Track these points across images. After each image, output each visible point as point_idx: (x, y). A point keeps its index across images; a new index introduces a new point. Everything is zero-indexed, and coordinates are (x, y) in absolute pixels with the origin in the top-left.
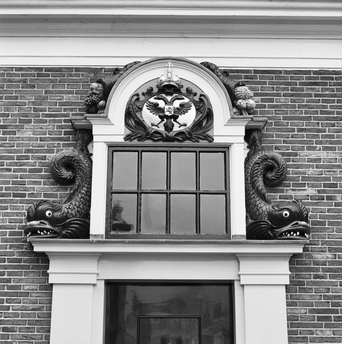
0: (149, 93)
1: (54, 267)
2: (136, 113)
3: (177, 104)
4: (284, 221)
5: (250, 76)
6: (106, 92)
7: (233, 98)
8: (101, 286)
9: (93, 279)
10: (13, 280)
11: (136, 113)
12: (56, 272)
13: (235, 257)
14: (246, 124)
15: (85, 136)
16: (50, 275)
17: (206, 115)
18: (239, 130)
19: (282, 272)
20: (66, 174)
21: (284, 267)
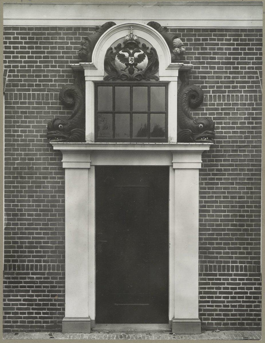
0: (119, 48)
3: (136, 55)
7: (172, 46)
9: (88, 166)
16: (67, 172)
17: (154, 63)
20: (69, 101)
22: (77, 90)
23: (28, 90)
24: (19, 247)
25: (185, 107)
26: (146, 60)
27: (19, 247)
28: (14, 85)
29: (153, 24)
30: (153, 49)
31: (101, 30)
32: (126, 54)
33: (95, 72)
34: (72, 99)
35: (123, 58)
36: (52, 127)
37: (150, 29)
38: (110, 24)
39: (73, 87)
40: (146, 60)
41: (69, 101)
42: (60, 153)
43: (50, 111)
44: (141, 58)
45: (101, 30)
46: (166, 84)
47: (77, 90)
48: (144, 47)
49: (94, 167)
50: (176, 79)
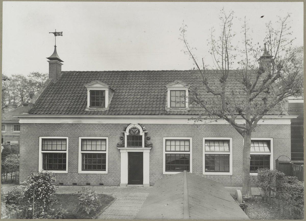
0: (132, 129)
1: (121, 151)
2: (184, 101)
3: (135, 130)
4: (149, 145)
5: (144, 125)
6: (126, 128)
7: (143, 129)
8: (127, 153)
9: (126, 152)
10: (125, 131)
11: (184, 101)
12: (121, 151)
13: (143, 149)
14: (298, 116)
15: (124, 134)
16: (121, 153)
17: (139, 132)
18: (144, 134)
19: (149, 151)
20: (122, 139)
21: (149, 150)
22: (146, 140)
23: (113, 136)
24: (111, 169)
25: (7, 99)
26: (137, 131)
27: (111, 169)
28: (110, 135)
29: (139, 124)
30: (139, 129)
31: (129, 125)
32: (133, 130)
33: (127, 133)
34: (122, 138)
35: (132, 131)
36: (118, 144)
37: (134, 149)
38: (130, 124)
39: (122, 136)
40: (137, 131)
41: (122, 139)
42: (120, 150)
43: (118, 141)
44: (136, 131)
45: (129, 125)
46: (141, 136)
47: (123, 137)
48: (137, 129)
49: (170, 91)
50: (144, 135)
